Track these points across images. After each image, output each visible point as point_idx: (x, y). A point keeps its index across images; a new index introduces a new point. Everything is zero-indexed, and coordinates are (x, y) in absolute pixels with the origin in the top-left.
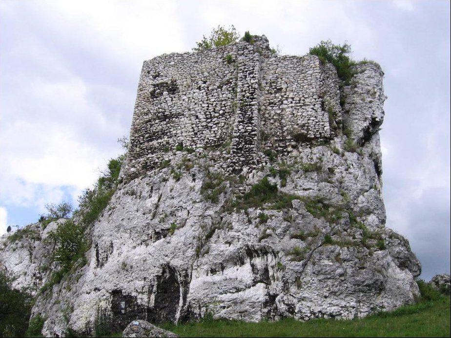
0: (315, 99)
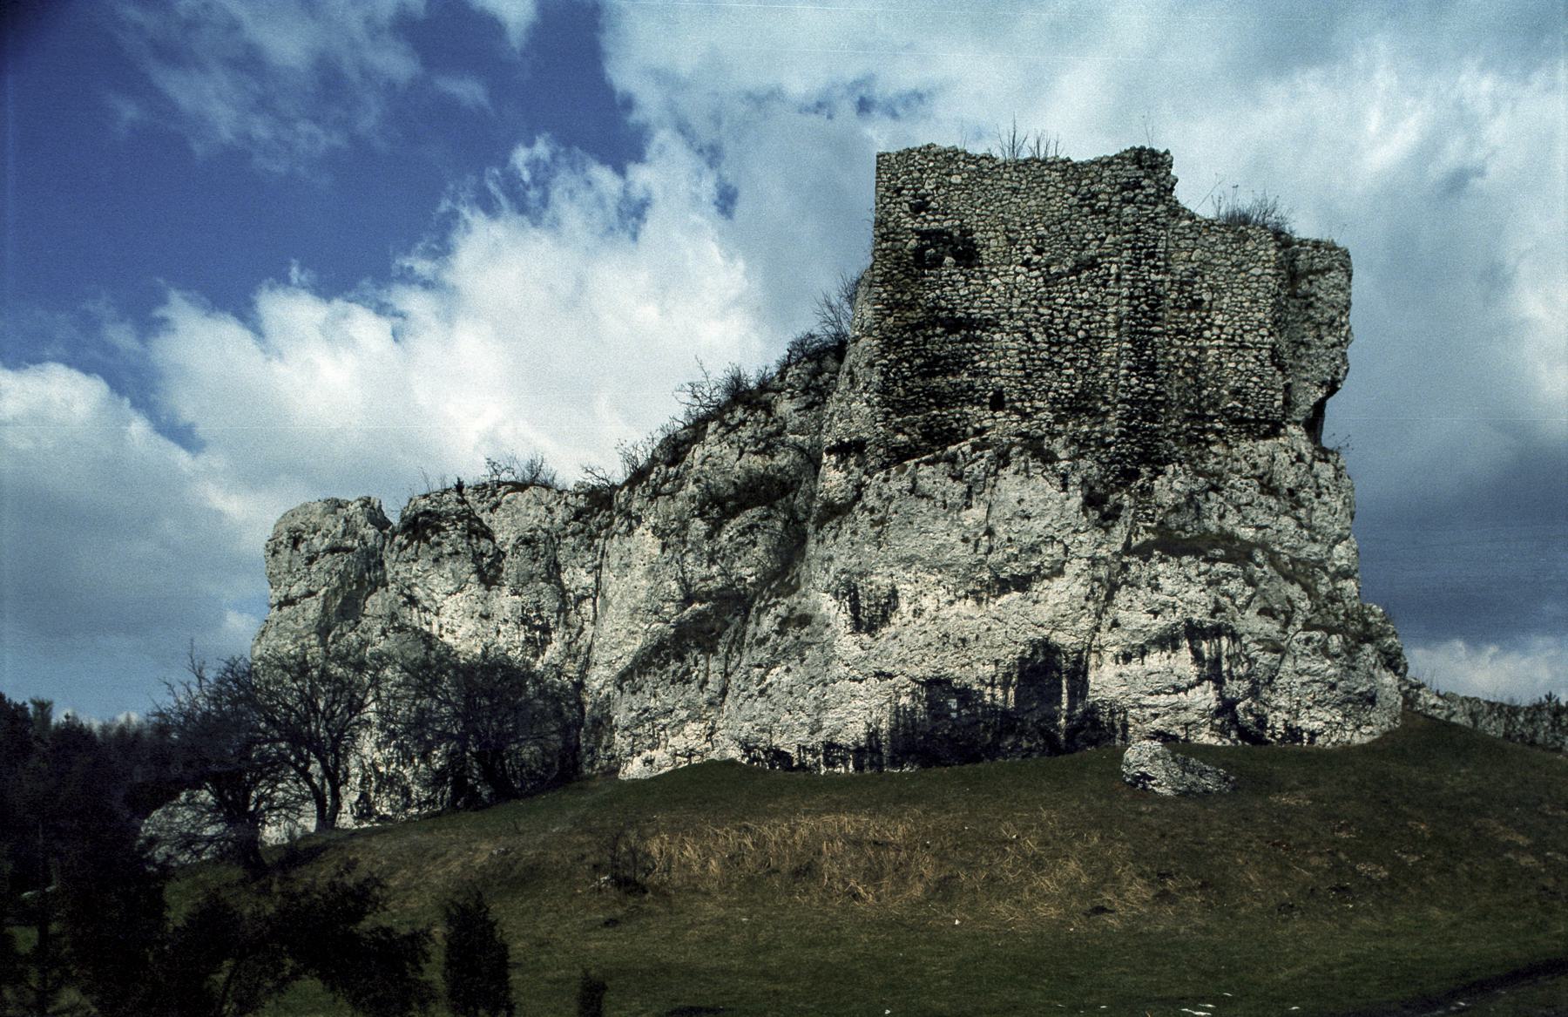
0: (1263, 337)
